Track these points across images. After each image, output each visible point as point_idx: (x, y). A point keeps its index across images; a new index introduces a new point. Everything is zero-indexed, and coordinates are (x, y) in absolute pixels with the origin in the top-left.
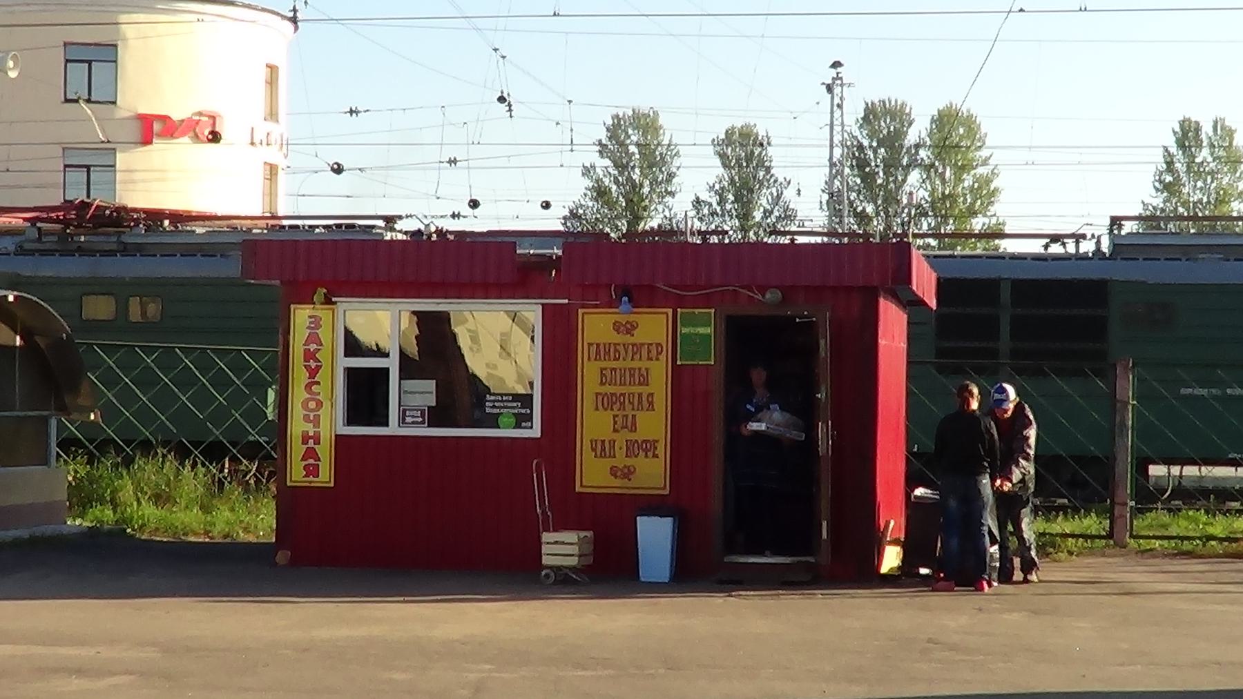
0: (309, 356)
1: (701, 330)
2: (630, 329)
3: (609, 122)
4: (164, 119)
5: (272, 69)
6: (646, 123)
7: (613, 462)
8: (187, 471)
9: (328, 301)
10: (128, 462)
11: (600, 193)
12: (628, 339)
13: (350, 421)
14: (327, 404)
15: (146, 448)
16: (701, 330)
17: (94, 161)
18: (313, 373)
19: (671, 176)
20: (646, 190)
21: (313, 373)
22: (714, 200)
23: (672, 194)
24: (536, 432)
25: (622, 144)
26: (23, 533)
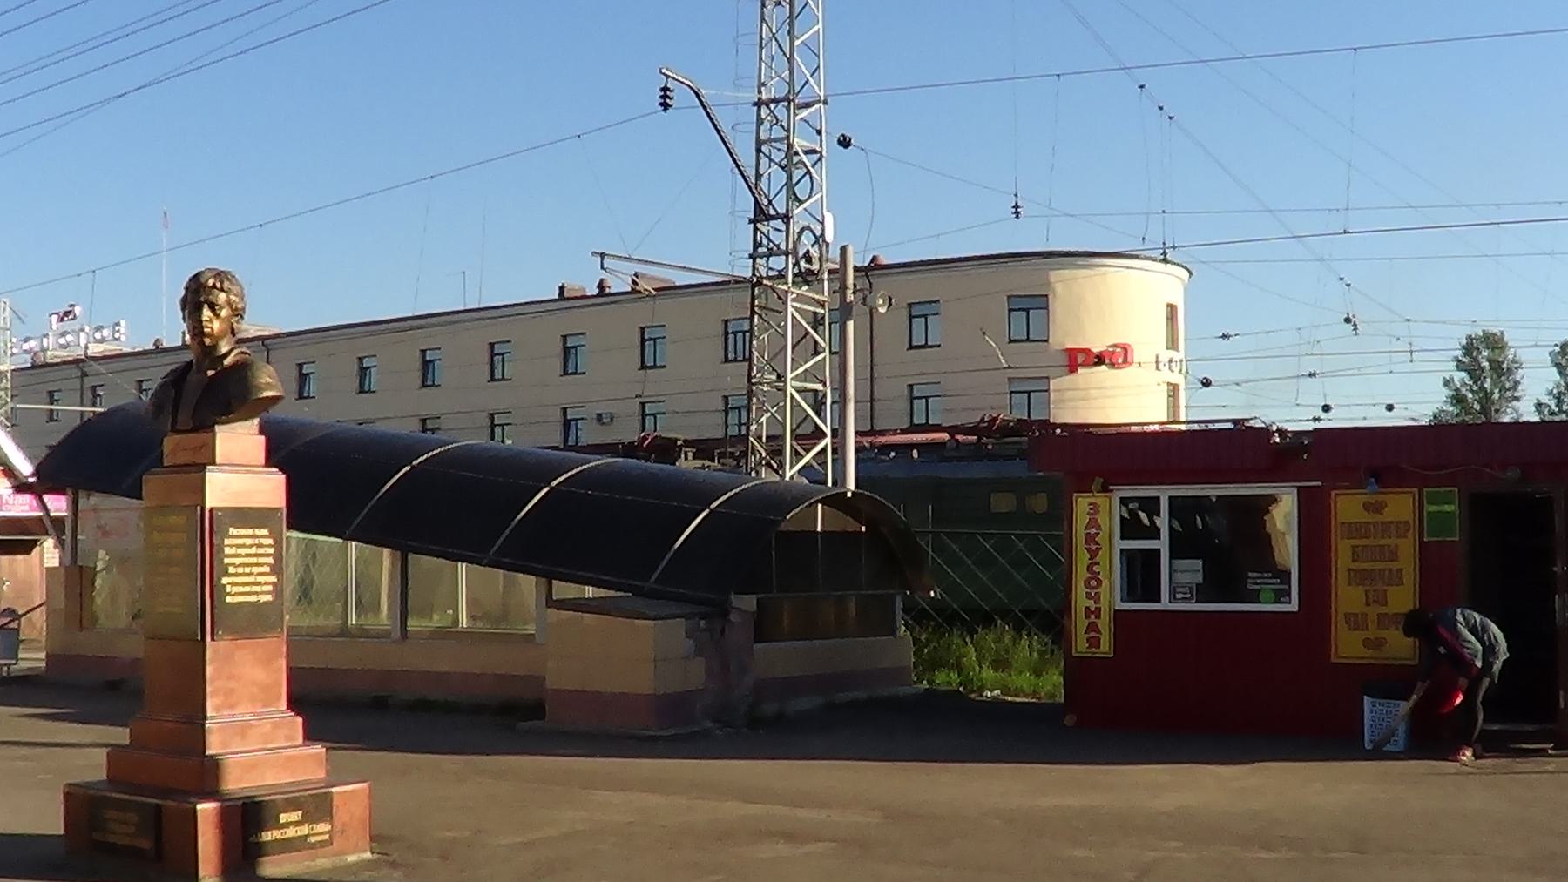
0: (1090, 539)
1: (1447, 508)
2: (1378, 508)
3: (1464, 342)
4: (1087, 351)
5: (1172, 309)
6: (1494, 342)
7: (1366, 635)
8: (1025, 642)
9: (1105, 489)
10: (972, 632)
11: (1458, 399)
12: (1378, 518)
13: (1130, 595)
14: (1105, 583)
15: (987, 621)
16: (1447, 508)
17: (1034, 388)
18: (1093, 554)
19: (1517, 383)
20: (1496, 396)
21: (1093, 554)
22: (1553, 403)
23: (1517, 399)
24: (1293, 606)
25: (1476, 359)
26: (861, 695)
